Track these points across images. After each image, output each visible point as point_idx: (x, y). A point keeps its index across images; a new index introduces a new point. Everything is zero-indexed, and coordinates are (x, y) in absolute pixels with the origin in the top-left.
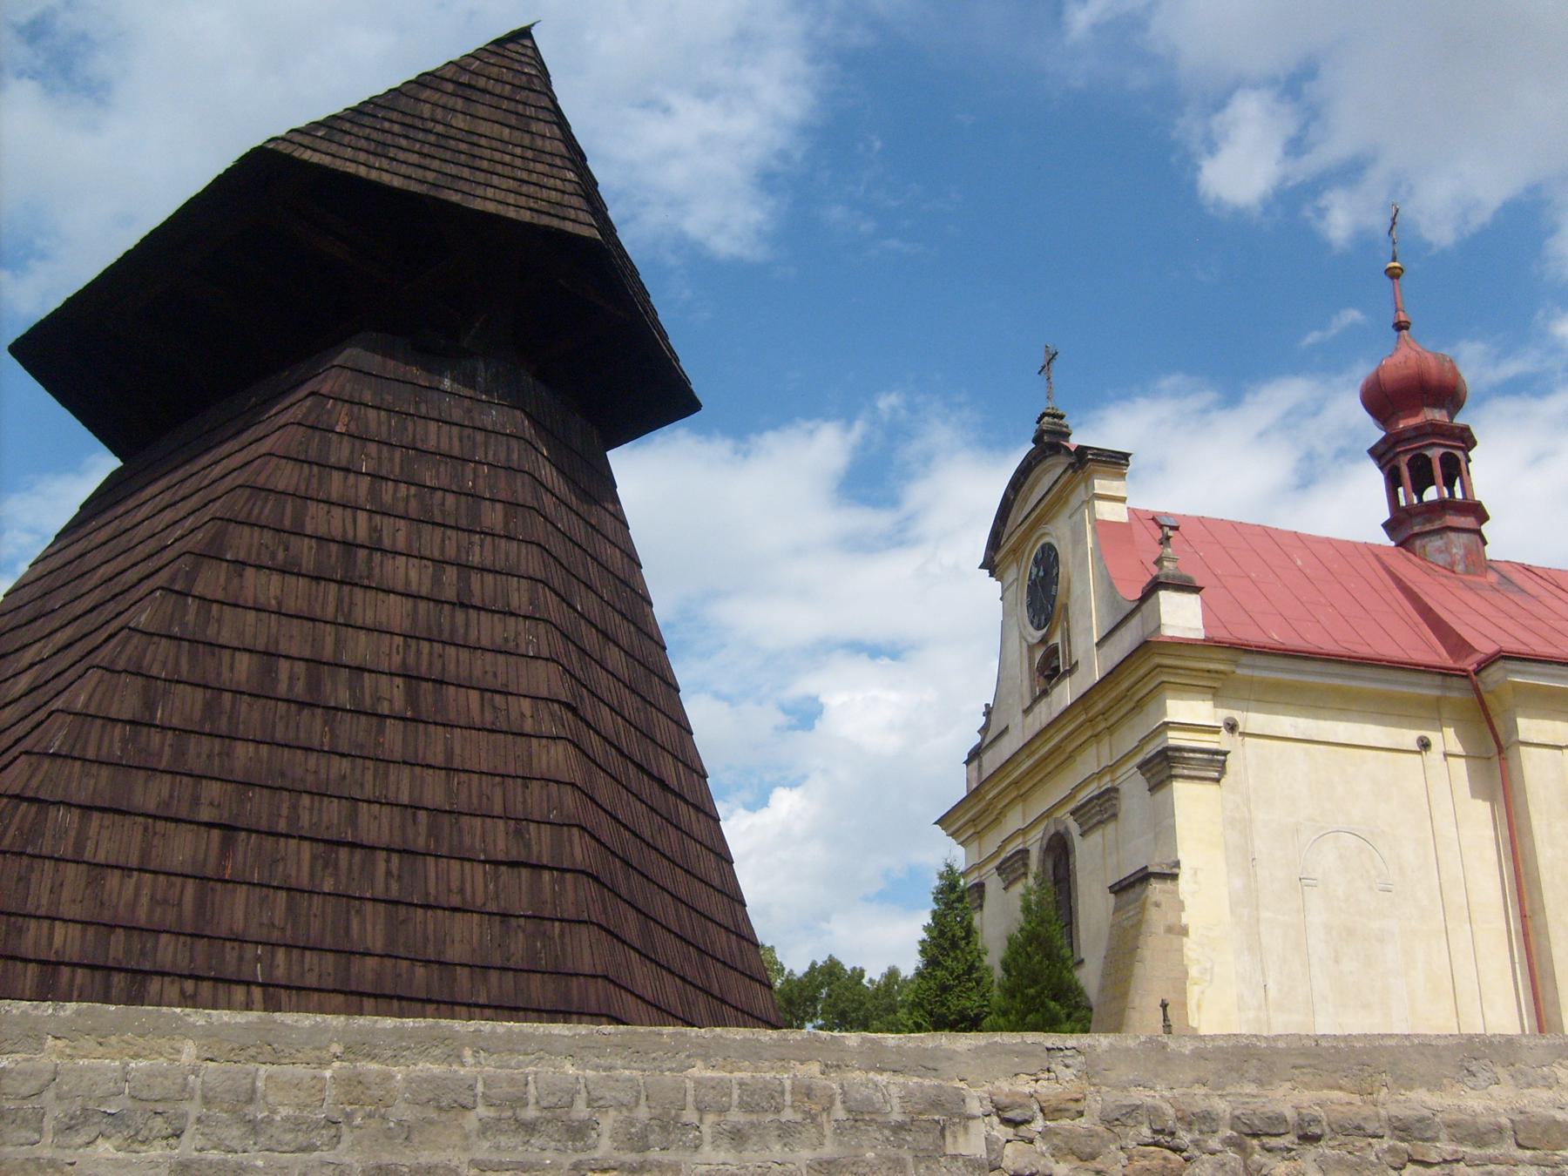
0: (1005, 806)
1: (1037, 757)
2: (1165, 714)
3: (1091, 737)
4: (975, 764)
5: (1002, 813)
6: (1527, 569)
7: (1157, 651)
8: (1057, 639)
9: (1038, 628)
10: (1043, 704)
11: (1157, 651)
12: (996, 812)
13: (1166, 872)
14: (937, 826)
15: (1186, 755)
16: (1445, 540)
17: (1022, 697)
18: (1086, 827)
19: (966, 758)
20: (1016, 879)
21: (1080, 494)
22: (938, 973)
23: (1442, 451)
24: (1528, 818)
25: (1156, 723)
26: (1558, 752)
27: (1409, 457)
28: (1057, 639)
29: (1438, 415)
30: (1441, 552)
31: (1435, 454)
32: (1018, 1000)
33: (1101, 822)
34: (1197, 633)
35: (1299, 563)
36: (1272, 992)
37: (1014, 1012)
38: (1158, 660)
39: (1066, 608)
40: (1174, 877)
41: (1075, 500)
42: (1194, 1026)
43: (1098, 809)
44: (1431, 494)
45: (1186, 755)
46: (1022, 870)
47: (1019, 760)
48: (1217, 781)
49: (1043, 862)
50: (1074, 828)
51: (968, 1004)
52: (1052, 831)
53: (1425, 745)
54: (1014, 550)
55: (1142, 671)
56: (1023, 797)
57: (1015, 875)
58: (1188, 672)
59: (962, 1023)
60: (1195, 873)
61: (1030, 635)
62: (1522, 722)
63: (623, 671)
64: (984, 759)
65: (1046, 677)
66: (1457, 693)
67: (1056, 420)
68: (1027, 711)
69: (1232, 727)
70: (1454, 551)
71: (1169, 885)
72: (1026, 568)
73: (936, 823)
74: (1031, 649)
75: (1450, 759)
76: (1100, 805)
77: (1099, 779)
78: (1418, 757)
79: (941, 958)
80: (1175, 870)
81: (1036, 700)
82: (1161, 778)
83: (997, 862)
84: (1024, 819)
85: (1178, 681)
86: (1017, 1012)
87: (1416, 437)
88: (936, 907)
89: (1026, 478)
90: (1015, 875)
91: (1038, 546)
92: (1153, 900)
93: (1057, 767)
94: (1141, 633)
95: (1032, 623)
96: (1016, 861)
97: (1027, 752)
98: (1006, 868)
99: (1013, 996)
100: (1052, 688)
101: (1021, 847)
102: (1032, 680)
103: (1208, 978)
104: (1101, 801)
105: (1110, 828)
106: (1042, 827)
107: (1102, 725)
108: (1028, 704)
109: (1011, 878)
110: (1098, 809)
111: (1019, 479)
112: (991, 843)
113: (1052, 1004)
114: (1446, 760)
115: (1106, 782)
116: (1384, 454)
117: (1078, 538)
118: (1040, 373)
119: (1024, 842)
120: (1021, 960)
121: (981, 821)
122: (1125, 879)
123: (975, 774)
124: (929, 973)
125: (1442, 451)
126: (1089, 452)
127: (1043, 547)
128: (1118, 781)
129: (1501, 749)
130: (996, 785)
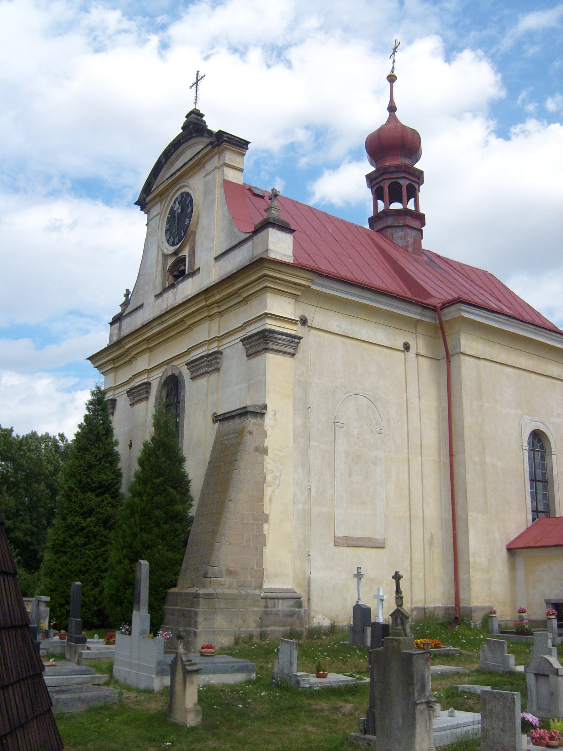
0: (137, 354)
1: (164, 325)
2: (265, 307)
3: (206, 317)
4: (117, 325)
5: (134, 357)
6: (438, 256)
7: (267, 266)
8: (186, 252)
9: (173, 245)
10: (170, 293)
11: (267, 266)
12: (130, 357)
13: (258, 411)
14: (89, 360)
15: (276, 336)
16: (404, 233)
17: (155, 287)
18: (196, 374)
19: (111, 321)
20: (141, 400)
21: (215, 162)
22: (87, 456)
23: (408, 182)
24: (461, 398)
25: (257, 314)
26: (477, 361)
27: (390, 183)
28: (186, 252)
29: (406, 161)
30: (401, 239)
31: (404, 183)
32: (149, 486)
33: (207, 372)
34: (289, 259)
35: (330, 230)
36: (313, 493)
37: (145, 495)
38: (266, 272)
39: (194, 233)
40: (263, 415)
41: (209, 166)
42: (267, 513)
43: (206, 363)
44: (396, 206)
45: (276, 336)
46: (145, 395)
47: (152, 326)
48: (293, 355)
49: (160, 392)
50: (186, 373)
51: (105, 477)
52: (170, 374)
53: (407, 347)
54: (161, 195)
55: (254, 278)
56: (150, 350)
57: (139, 398)
58: (283, 283)
59: (100, 488)
60: (275, 414)
61: (166, 248)
62: (463, 341)
63: (23, 692)
64: (123, 323)
65: (174, 276)
66: (428, 318)
67: (198, 117)
68: (157, 296)
69: (304, 321)
70: (409, 239)
71: (258, 420)
72: (169, 204)
73: (88, 359)
74: (166, 257)
75: (419, 358)
76: (208, 361)
77: (210, 344)
78: (402, 354)
79: (89, 446)
80: (264, 411)
81: (165, 290)
82: (258, 350)
83: (128, 387)
84: (149, 363)
85: (276, 287)
86: (148, 495)
87: (395, 172)
88: (87, 413)
89: (175, 151)
90: (139, 398)
91: (179, 193)
92: (249, 429)
93: (177, 334)
94: (251, 254)
95: (168, 241)
96: (142, 390)
97: (159, 322)
98: (133, 393)
99: (145, 483)
100: (178, 283)
101: (145, 381)
102: (164, 276)
103: (277, 482)
104: (209, 359)
105: (213, 377)
106: (163, 369)
107: (216, 310)
108: (158, 292)
109: (136, 399)
110: (206, 363)
111: (170, 150)
112: (124, 375)
113: (171, 490)
114: (417, 357)
115: (214, 348)
116: (375, 179)
117: (208, 191)
118: (191, 87)
119: (148, 378)
120: (153, 460)
121: (118, 361)
122: (228, 413)
123: (116, 331)
124: (81, 455)
125: (408, 182)
126: (225, 135)
127: (182, 194)
128: (223, 348)
129: (448, 357)
130: (108, 355)
